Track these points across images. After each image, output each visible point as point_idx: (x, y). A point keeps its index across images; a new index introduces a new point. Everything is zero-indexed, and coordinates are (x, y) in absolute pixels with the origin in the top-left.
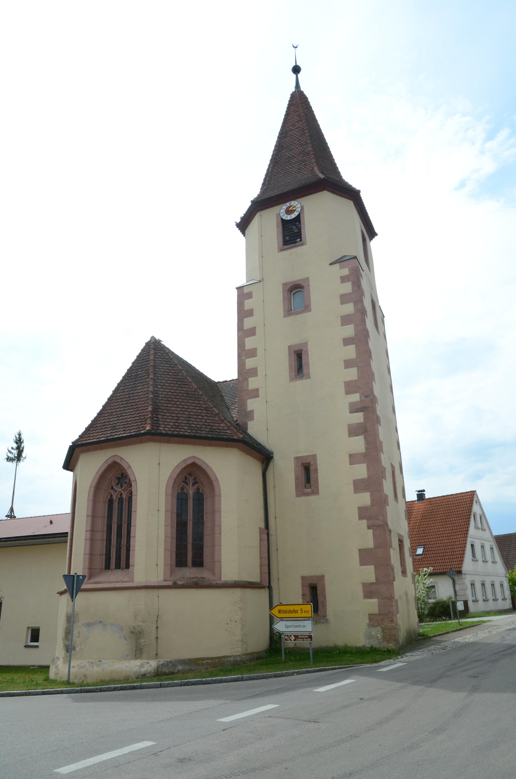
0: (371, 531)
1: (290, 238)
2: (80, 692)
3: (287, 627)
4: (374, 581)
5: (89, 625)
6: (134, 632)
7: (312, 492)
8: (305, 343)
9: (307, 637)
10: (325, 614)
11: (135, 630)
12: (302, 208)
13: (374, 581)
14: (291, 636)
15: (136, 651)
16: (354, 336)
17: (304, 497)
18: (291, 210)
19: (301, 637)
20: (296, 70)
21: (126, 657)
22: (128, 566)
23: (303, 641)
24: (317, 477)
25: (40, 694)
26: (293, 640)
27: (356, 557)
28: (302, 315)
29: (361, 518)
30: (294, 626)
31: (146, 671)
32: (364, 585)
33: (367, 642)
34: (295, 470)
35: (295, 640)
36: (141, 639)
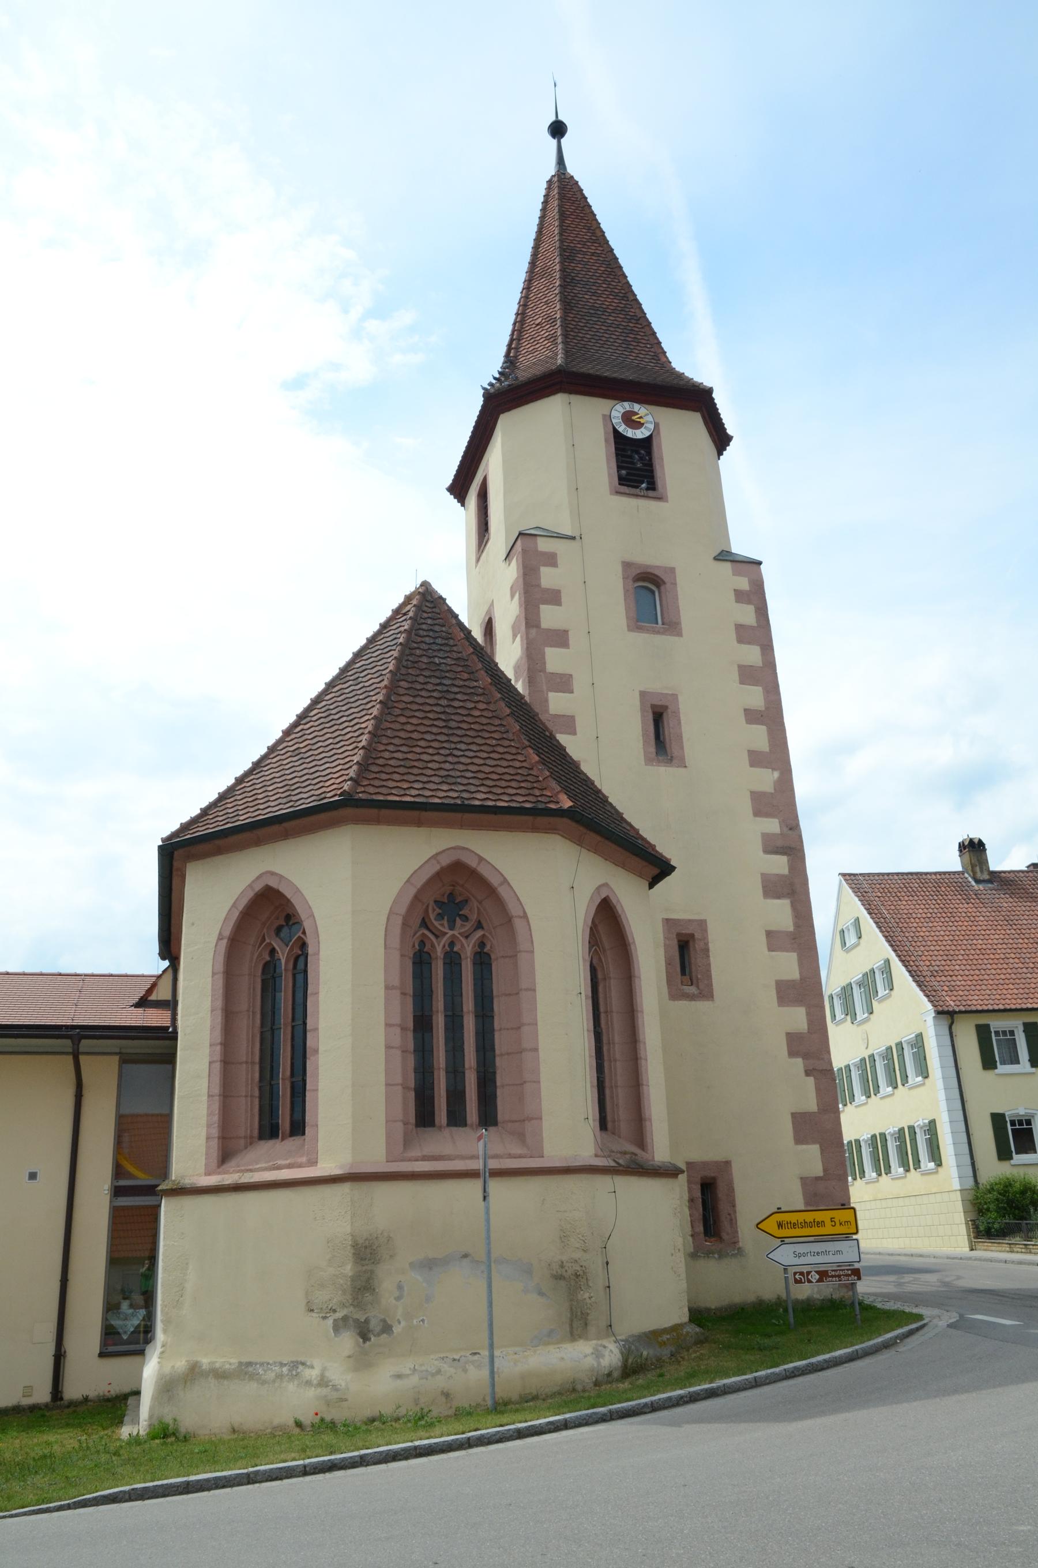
0: (811, 1080)
1: (628, 474)
2: (609, 1418)
3: (799, 1255)
4: (821, 1174)
5: (429, 1265)
6: (561, 1275)
7: (700, 993)
8: (673, 694)
9: (850, 1272)
10: (734, 1237)
11: (564, 1270)
12: (657, 426)
13: (821, 1174)
14: (809, 1273)
15: (572, 1321)
16: (763, 709)
17: (685, 1002)
18: (634, 421)
19: (833, 1273)
20: (558, 129)
21: (547, 1338)
22: (298, 1128)
23: (840, 1281)
24: (709, 965)
25: (511, 1436)
26: (814, 1281)
27: (787, 1127)
28: (664, 637)
29: (792, 1053)
30: (812, 1254)
31: (610, 1365)
32: (804, 1181)
33: (816, 1290)
34: (665, 945)
35: (820, 1280)
36: (582, 1292)
